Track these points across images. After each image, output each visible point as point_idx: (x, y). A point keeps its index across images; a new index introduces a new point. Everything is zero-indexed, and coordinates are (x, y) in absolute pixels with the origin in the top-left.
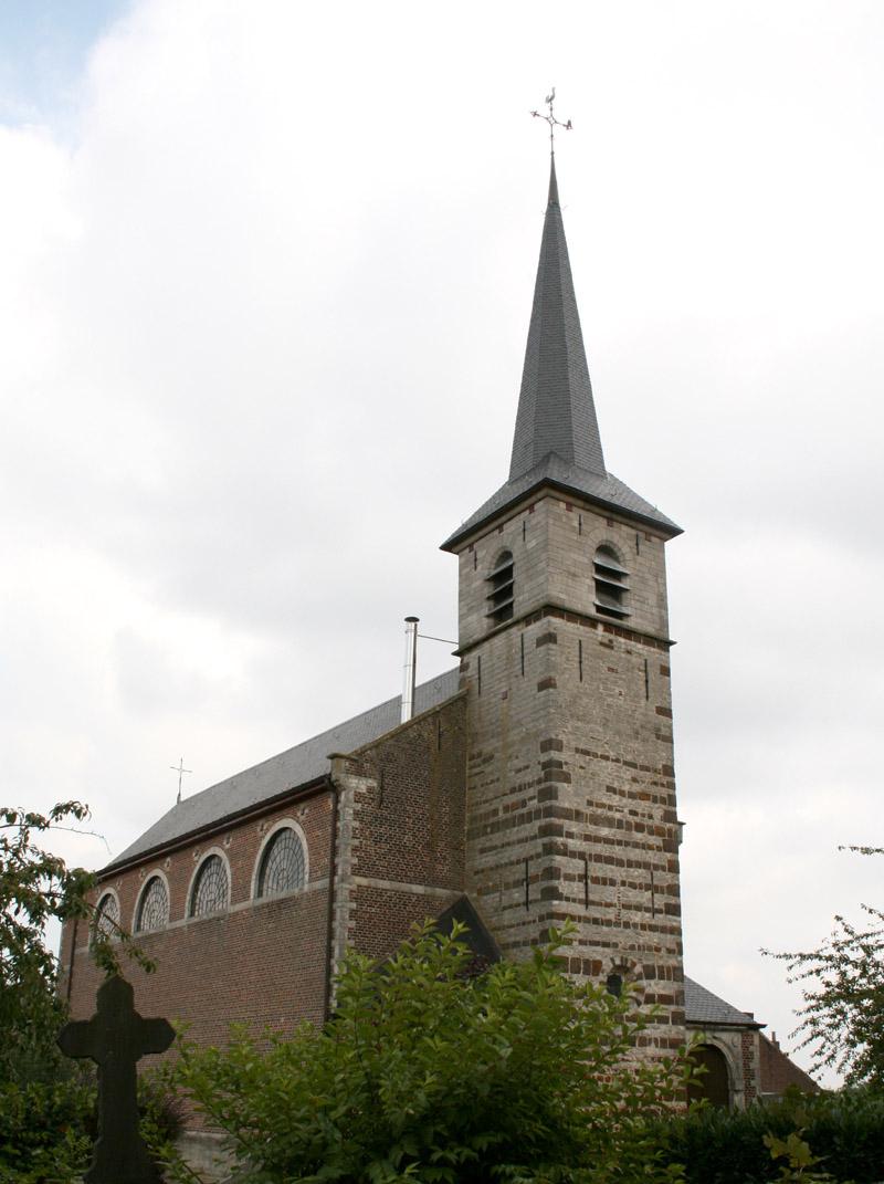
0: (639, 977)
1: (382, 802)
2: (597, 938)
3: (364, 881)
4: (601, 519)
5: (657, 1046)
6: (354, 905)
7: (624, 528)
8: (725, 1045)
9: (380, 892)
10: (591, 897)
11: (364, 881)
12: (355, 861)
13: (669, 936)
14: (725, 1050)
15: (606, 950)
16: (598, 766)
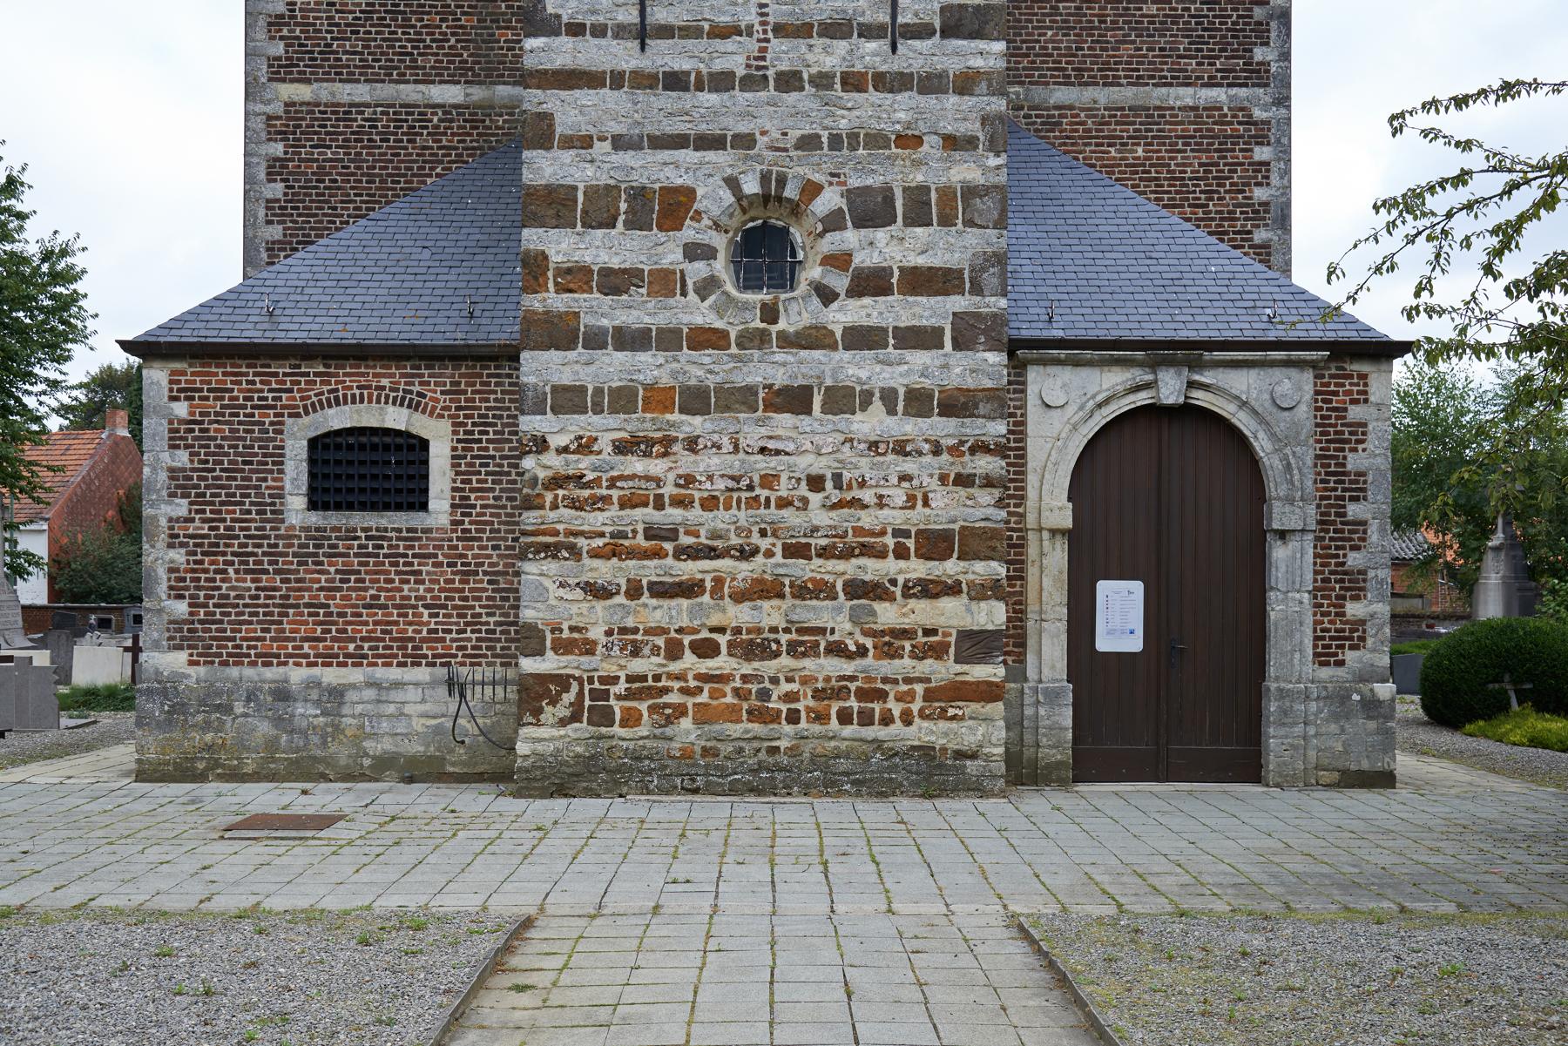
0: (833, 222)
2: (679, 127)
3: (302, 92)
5: (892, 411)
6: (278, 149)
8: (1244, 404)
9: (346, 112)
11: (302, 92)
12: (279, 49)
13: (952, 100)
15: (711, 156)
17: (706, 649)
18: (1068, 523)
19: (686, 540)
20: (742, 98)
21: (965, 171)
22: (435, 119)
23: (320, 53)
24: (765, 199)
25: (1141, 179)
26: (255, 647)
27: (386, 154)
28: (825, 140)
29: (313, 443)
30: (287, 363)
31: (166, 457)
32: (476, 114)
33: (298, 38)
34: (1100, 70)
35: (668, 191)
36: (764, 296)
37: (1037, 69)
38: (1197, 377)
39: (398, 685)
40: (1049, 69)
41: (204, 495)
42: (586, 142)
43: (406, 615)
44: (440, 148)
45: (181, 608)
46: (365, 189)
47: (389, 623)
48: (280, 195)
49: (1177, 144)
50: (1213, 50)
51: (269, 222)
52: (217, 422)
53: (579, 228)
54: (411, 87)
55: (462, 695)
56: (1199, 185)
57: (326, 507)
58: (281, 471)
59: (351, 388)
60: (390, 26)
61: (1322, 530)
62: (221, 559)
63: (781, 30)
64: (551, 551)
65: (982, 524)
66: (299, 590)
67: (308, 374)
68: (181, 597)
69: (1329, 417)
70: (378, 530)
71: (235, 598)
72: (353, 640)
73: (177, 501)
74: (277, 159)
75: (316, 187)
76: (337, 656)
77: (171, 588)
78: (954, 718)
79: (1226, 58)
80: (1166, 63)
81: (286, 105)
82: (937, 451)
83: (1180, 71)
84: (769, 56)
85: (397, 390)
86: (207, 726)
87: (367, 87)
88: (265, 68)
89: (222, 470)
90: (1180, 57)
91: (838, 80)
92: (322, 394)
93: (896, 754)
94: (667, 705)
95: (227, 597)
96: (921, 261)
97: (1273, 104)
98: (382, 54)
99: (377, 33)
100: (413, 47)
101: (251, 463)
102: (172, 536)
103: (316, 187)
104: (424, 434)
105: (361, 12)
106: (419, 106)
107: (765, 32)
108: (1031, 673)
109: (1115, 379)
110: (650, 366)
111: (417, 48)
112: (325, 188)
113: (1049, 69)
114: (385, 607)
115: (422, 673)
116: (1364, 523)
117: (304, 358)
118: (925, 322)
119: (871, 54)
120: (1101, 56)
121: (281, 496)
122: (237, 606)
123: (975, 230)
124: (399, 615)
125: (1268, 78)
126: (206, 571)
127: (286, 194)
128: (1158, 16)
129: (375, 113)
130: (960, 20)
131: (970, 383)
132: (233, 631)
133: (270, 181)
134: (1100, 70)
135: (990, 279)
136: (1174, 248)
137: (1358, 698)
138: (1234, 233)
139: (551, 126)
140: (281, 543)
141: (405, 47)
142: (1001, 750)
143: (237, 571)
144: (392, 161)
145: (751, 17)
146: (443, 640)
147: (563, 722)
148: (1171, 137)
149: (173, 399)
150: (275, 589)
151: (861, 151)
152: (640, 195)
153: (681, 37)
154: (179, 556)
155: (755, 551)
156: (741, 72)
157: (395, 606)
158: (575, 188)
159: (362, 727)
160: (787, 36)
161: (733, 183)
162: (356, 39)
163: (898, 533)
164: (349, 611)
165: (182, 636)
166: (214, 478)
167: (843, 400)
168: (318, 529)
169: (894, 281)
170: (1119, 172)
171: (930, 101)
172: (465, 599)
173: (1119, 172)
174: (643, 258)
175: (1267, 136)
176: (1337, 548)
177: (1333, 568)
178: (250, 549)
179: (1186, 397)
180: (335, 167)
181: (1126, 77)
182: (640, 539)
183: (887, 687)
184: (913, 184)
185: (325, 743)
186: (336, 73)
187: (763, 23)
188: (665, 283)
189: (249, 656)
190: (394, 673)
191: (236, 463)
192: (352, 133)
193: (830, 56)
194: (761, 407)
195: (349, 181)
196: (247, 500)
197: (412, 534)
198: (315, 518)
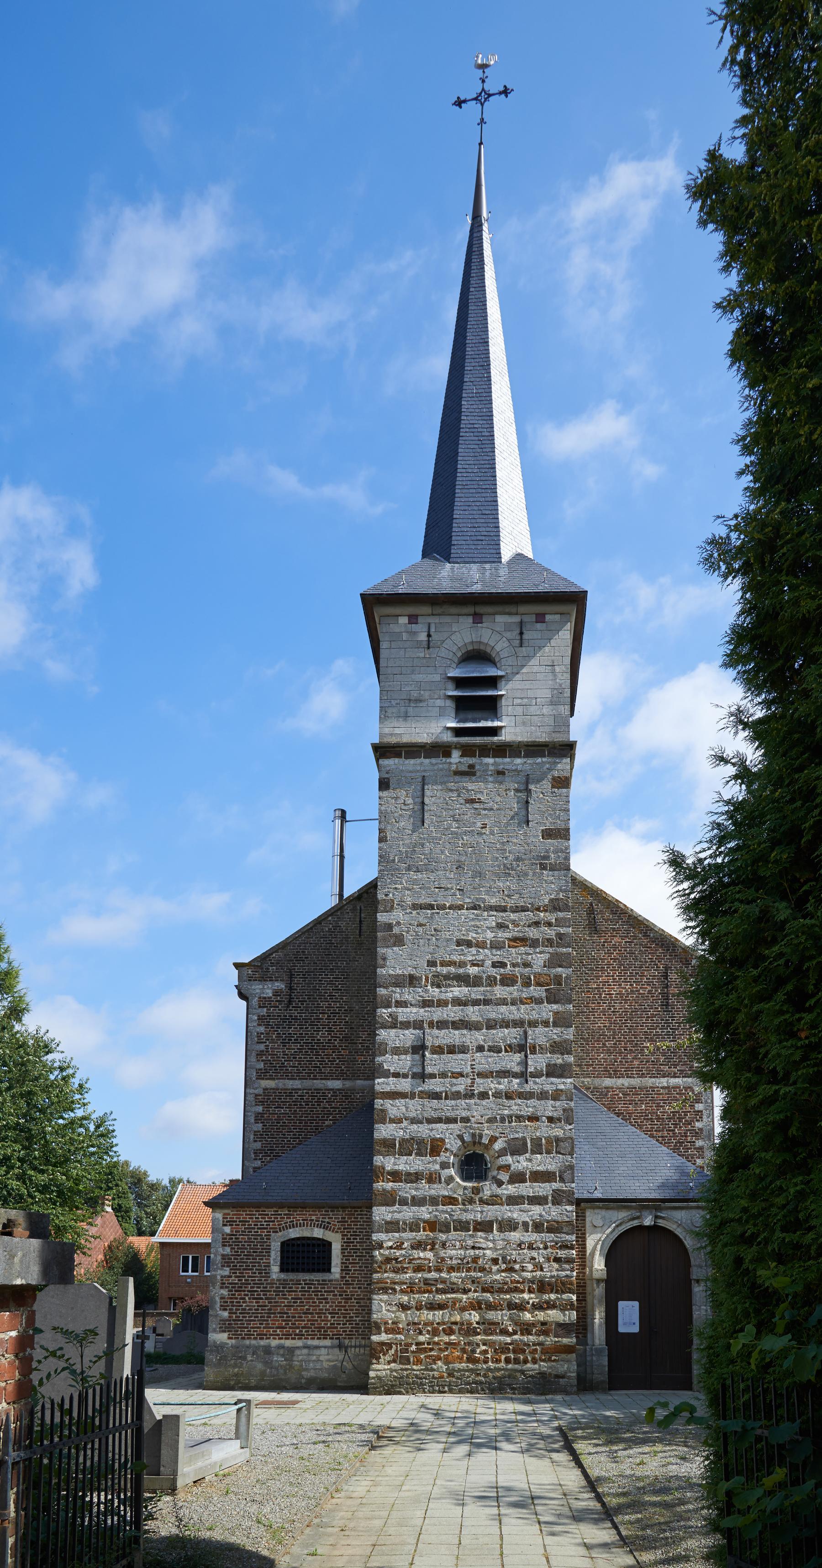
0: (502, 1153)
1: (290, 1002)
3: (270, 1084)
4: (461, 619)
6: (260, 1109)
7: (500, 619)
9: (290, 1093)
10: (429, 1070)
11: (270, 1084)
14: (679, 1232)
15: (452, 1126)
16: (441, 920)
17: (450, 1332)
19: (440, 1286)
20: (463, 1103)
29: (283, 1244)
31: (220, 1250)
35: (434, 1140)
39: (317, 1347)
42: (400, 1121)
45: (226, 1314)
48: (260, 1129)
51: (255, 1141)
54: (319, 1081)
55: (346, 1351)
57: (287, 1271)
58: (269, 1256)
63: (481, 1075)
64: (385, 1290)
68: (225, 1310)
72: (298, 1328)
77: (221, 1306)
78: (555, 1361)
82: (546, 1248)
86: (235, 1366)
87: (300, 1082)
94: (431, 1356)
95: (245, 1309)
96: (540, 1168)
104: (329, 1240)
108: (589, 1342)
109: (623, 1214)
110: (425, 1213)
114: (312, 1313)
115: (328, 1342)
118: (541, 1194)
121: (269, 1266)
126: (236, 1298)
135: (567, 1176)
142: (574, 1374)
145: (469, 1069)
146: (336, 1328)
147: (389, 1363)
149: (224, 1225)
150: (265, 1306)
151: (514, 1124)
152: (421, 1142)
154: (225, 1292)
155: (470, 1290)
159: (302, 1365)
161: (461, 1137)
165: (226, 1326)
167: (509, 1225)
168: (284, 1280)
172: (346, 1310)
182: (422, 1285)
185: (285, 1373)
187: (473, 1072)
188: (432, 1178)
190: (316, 1342)
193: (503, 1085)
197: (324, 1283)
198: (283, 1276)
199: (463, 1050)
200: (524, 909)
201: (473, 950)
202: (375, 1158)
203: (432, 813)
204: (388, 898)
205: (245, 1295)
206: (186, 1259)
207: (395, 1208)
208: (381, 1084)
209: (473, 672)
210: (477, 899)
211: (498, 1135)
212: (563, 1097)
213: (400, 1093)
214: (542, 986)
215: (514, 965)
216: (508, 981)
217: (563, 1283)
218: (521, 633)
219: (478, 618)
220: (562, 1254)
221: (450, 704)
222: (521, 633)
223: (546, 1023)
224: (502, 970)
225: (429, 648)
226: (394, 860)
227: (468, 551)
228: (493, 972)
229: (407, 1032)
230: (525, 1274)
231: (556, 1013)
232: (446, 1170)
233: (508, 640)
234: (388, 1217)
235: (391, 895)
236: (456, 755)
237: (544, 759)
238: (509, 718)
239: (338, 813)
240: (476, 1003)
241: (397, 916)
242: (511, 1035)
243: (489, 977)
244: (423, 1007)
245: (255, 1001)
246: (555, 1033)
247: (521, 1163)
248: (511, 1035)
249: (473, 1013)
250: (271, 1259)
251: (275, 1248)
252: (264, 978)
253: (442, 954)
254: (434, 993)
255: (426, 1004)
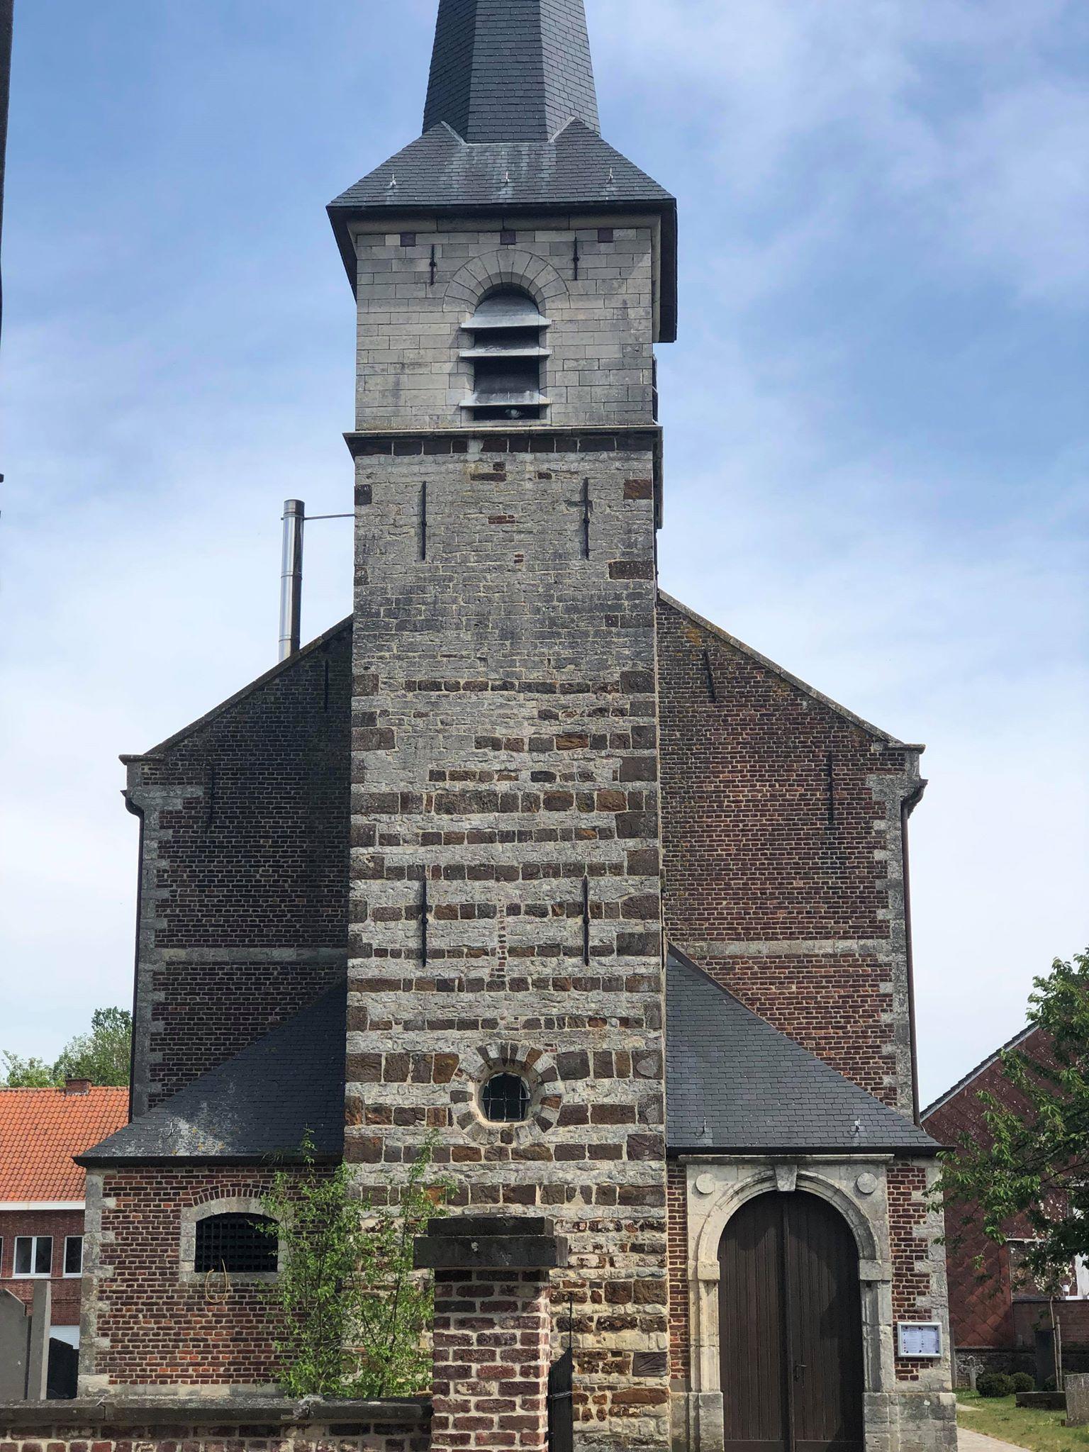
0: (549, 1076)
1: (211, 819)
2: (449, 1015)
3: (180, 954)
5: (588, 1202)
6: (161, 996)
9: (210, 969)
11: (180, 954)
12: (164, 924)
15: (468, 1033)
16: (451, 705)
18: (716, 1275)
20: (487, 996)
21: (634, 1042)
22: (275, 973)
23: (193, 926)
24: (504, 1061)
25: (795, 1008)
26: (156, 1371)
27: (239, 999)
28: (542, 1022)
29: (200, 1224)
30: (184, 1169)
31: (99, 1236)
32: (305, 969)
33: (178, 916)
34: (762, 929)
35: (441, 1057)
36: (503, 1125)
37: (716, 929)
38: (803, 1172)
40: (724, 929)
41: (124, 1263)
42: (387, 1026)
43: (260, 1346)
44: (278, 994)
46: (224, 1024)
47: (249, 1352)
49: (822, 982)
50: (846, 912)
51: (153, 1050)
52: (135, 1211)
53: (383, 1082)
54: (258, 950)
56: (839, 1012)
58: (177, 1245)
59: (227, 1186)
60: (244, 906)
61: (897, 1281)
62: (134, 1307)
63: (513, 951)
65: (650, 1279)
66: (188, 1328)
67: (198, 1177)
68: (105, 1335)
69: (899, 1199)
70: (242, 1285)
71: (143, 1335)
72: (223, 1364)
73: (105, 1266)
74: (161, 1004)
75: (188, 1024)
76: (211, 1376)
77: (99, 1329)
79: (856, 918)
80: (812, 923)
81: (168, 964)
82: (618, 1228)
83: (822, 928)
84: (506, 968)
85: (258, 1187)
88: (153, 938)
89: (137, 1245)
90: (821, 918)
91: (551, 983)
92: (207, 1190)
93: (595, 1441)
95: (137, 1335)
96: (607, 1101)
97: (893, 951)
98: (238, 926)
99: (234, 911)
100: (260, 921)
101: (157, 1239)
102: (103, 1292)
103: (188, 1024)
105: (223, 896)
106: (264, 964)
107: (503, 953)
111: (264, 921)
112: (194, 1024)
113: (724, 929)
114: (246, 1340)
116: (927, 1275)
117: (195, 1166)
118: (610, 1142)
119: (571, 965)
120: (763, 918)
121: (177, 1262)
122: (144, 1341)
123: (642, 1080)
124: (255, 1346)
125: (888, 932)
126: (123, 1316)
127: (166, 1029)
128: (804, 888)
129: (232, 969)
130: (630, 942)
131: (640, 1182)
132: (140, 1359)
133: (154, 1020)
134: (762, 929)
135: (652, 1112)
136: (799, 1074)
137: (928, 1403)
138: (867, 1047)
139: (365, 1016)
140: (176, 1295)
141: (255, 921)
143: (144, 1317)
144: (244, 1004)
148: (817, 977)
149: (106, 1195)
150: (170, 1328)
151: (566, 1029)
152: (421, 1059)
153: (449, 957)
154: (105, 1306)
156: (487, 979)
157: (253, 1340)
158: (380, 1056)
160: (518, 956)
161: (483, 1051)
162: (220, 916)
163: (593, 1285)
164: (221, 1343)
166: (132, 1250)
169: (589, 1114)
170: (779, 1004)
171: (611, 996)
173: (779, 1004)
174: (424, 1101)
175: (889, 975)
176: (909, 1293)
177: (906, 1308)
178: (154, 1300)
179: (797, 1186)
180: (202, 1009)
181: (782, 933)
183: (588, 1393)
184: (600, 1050)
186: (204, 941)
187: (502, 947)
189: (151, 1376)
191: (147, 1239)
192: (215, 984)
193: (549, 967)
194: (502, 1200)
195: (212, 1019)
196: (154, 1266)
198: (198, 1277)
199: (487, 912)
200: (582, 689)
201: (503, 754)
202: (348, 1085)
203: (437, 539)
204: (369, 672)
205: (137, 1310)
206: (25, 1244)
207: (378, 1166)
208: (359, 967)
209: (501, 322)
210: (508, 674)
211: (541, 1047)
212: (645, 986)
213: (386, 981)
214: (610, 809)
215: (567, 777)
216: (556, 802)
217: (647, 1286)
218: (576, 260)
219: (508, 237)
220: (647, 1237)
221: (467, 369)
222: (576, 260)
223: (616, 869)
224: (548, 785)
225: (432, 283)
226: (378, 614)
227: (493, 122)
228: (536, 788)
229: (398, 884)
230: (584, 1271)
231: (632, 854)
232: (460, 1105)
233: (555, 270)
234: (371, 1181)
235: (373, 668)
236: (474, 448)
237: (612, 455)
238: (557, 390)
239: (292, 507)
240: (506, 837)
241: (383, 700)
242: (564, 888)
243: (527, 796)
244: (423, 845)
245: (154, 818)
246: (631, 886)
247: (580, 1092)
248: (566, 888)
249: (503, 854)
250: (182, 1250)
251: (188, 1230)
252: (169, 780)
253: (453, 762)
254: (444, 822)
255: (429, 839)
